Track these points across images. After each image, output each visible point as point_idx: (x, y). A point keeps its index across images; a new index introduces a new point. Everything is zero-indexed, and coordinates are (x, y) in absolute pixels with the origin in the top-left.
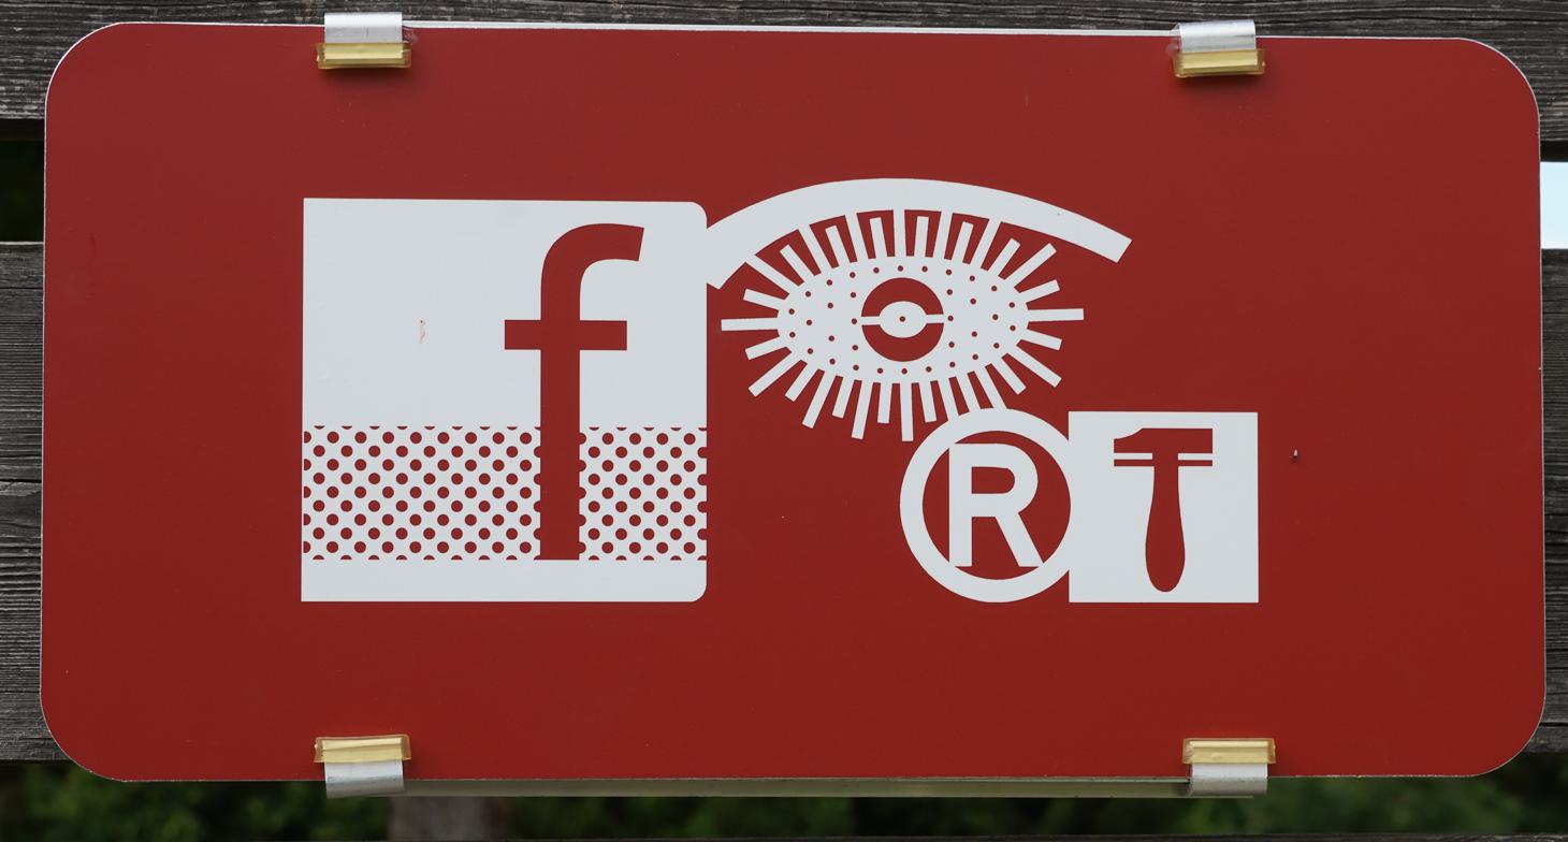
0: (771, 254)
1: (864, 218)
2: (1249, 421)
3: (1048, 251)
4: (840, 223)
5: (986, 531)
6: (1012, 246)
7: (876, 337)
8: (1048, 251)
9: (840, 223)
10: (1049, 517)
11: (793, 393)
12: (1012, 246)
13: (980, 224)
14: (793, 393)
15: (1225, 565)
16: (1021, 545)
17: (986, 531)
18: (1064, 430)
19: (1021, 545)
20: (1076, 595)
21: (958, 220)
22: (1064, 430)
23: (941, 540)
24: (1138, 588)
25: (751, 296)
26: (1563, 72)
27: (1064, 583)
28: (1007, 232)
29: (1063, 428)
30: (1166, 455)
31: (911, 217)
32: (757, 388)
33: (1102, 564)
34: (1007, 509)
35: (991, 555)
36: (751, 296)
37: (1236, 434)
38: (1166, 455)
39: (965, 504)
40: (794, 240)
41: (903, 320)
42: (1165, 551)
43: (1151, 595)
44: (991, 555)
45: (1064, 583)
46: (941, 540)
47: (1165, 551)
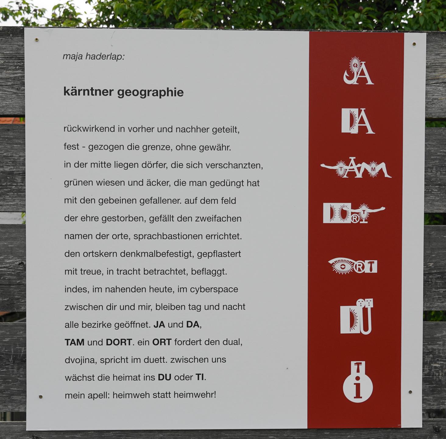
0: (335, 262)
1: (338, 261)
2: (377, 261)
3: (353, 263)
4: (340, 260)
5: (359, 268)
6: (350, 263)
7: (345, 266)
8: (353, 263)
9: (340, 260)
10: (363, 268)
11: (336, 271)
12: (350, 263)
13: (348, 261)
14: (336, 271)
15: (375, 270)
16: (361, 269)
17: (359, 268)
18: (364, 262)
19: (361, 269)
20: (365, 272)
21: (347, 261)
22: (364, 262)
23: (356, 269)
24: (369, 272)
25: (334, 264)
26: (1, 149)
27: (364, 272)
28: (350, 262)
29: (364, 262)
30: (371, 263)
31: (344, 260)
32: (333, 270)
33: (367, 270)
34: (360, 267)
35: (359, 270)
36: (334, 264)
37: (363, 363)
38: (371, 263)
39: (358, 267)
40: (337, 261)
41: (343, 267)
42: (371, 270)
43: (370, 272)
44: (359, 270)
45: (364, 272)
46: (356, 269)
47: (371, 270)
